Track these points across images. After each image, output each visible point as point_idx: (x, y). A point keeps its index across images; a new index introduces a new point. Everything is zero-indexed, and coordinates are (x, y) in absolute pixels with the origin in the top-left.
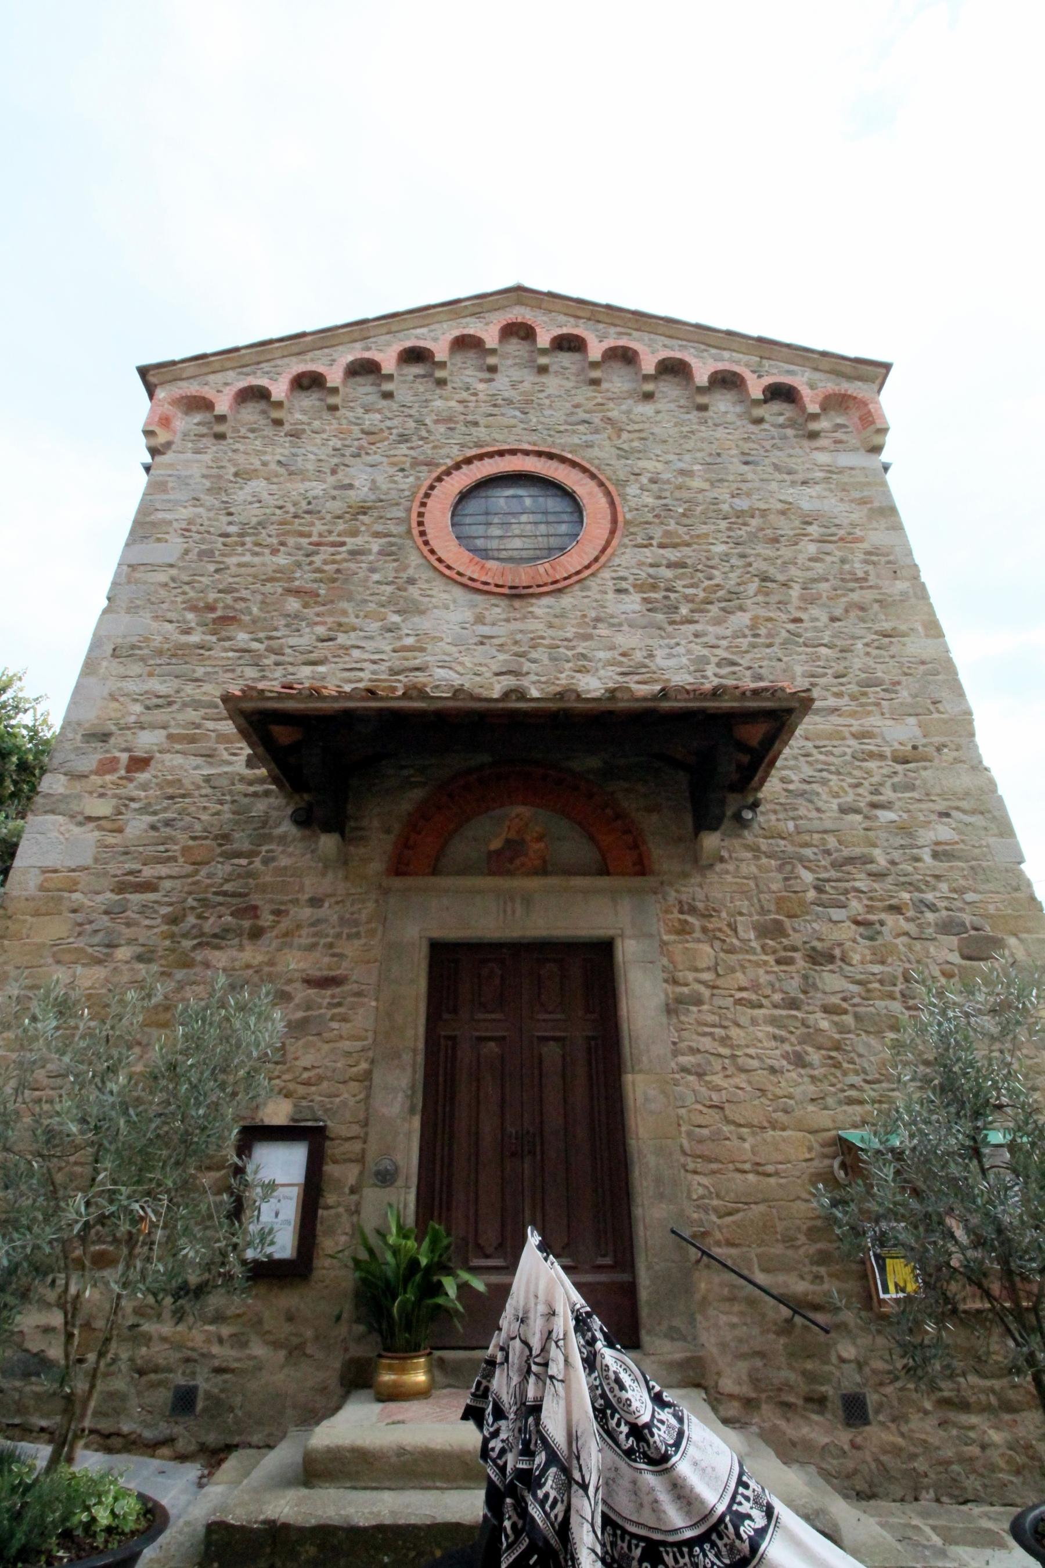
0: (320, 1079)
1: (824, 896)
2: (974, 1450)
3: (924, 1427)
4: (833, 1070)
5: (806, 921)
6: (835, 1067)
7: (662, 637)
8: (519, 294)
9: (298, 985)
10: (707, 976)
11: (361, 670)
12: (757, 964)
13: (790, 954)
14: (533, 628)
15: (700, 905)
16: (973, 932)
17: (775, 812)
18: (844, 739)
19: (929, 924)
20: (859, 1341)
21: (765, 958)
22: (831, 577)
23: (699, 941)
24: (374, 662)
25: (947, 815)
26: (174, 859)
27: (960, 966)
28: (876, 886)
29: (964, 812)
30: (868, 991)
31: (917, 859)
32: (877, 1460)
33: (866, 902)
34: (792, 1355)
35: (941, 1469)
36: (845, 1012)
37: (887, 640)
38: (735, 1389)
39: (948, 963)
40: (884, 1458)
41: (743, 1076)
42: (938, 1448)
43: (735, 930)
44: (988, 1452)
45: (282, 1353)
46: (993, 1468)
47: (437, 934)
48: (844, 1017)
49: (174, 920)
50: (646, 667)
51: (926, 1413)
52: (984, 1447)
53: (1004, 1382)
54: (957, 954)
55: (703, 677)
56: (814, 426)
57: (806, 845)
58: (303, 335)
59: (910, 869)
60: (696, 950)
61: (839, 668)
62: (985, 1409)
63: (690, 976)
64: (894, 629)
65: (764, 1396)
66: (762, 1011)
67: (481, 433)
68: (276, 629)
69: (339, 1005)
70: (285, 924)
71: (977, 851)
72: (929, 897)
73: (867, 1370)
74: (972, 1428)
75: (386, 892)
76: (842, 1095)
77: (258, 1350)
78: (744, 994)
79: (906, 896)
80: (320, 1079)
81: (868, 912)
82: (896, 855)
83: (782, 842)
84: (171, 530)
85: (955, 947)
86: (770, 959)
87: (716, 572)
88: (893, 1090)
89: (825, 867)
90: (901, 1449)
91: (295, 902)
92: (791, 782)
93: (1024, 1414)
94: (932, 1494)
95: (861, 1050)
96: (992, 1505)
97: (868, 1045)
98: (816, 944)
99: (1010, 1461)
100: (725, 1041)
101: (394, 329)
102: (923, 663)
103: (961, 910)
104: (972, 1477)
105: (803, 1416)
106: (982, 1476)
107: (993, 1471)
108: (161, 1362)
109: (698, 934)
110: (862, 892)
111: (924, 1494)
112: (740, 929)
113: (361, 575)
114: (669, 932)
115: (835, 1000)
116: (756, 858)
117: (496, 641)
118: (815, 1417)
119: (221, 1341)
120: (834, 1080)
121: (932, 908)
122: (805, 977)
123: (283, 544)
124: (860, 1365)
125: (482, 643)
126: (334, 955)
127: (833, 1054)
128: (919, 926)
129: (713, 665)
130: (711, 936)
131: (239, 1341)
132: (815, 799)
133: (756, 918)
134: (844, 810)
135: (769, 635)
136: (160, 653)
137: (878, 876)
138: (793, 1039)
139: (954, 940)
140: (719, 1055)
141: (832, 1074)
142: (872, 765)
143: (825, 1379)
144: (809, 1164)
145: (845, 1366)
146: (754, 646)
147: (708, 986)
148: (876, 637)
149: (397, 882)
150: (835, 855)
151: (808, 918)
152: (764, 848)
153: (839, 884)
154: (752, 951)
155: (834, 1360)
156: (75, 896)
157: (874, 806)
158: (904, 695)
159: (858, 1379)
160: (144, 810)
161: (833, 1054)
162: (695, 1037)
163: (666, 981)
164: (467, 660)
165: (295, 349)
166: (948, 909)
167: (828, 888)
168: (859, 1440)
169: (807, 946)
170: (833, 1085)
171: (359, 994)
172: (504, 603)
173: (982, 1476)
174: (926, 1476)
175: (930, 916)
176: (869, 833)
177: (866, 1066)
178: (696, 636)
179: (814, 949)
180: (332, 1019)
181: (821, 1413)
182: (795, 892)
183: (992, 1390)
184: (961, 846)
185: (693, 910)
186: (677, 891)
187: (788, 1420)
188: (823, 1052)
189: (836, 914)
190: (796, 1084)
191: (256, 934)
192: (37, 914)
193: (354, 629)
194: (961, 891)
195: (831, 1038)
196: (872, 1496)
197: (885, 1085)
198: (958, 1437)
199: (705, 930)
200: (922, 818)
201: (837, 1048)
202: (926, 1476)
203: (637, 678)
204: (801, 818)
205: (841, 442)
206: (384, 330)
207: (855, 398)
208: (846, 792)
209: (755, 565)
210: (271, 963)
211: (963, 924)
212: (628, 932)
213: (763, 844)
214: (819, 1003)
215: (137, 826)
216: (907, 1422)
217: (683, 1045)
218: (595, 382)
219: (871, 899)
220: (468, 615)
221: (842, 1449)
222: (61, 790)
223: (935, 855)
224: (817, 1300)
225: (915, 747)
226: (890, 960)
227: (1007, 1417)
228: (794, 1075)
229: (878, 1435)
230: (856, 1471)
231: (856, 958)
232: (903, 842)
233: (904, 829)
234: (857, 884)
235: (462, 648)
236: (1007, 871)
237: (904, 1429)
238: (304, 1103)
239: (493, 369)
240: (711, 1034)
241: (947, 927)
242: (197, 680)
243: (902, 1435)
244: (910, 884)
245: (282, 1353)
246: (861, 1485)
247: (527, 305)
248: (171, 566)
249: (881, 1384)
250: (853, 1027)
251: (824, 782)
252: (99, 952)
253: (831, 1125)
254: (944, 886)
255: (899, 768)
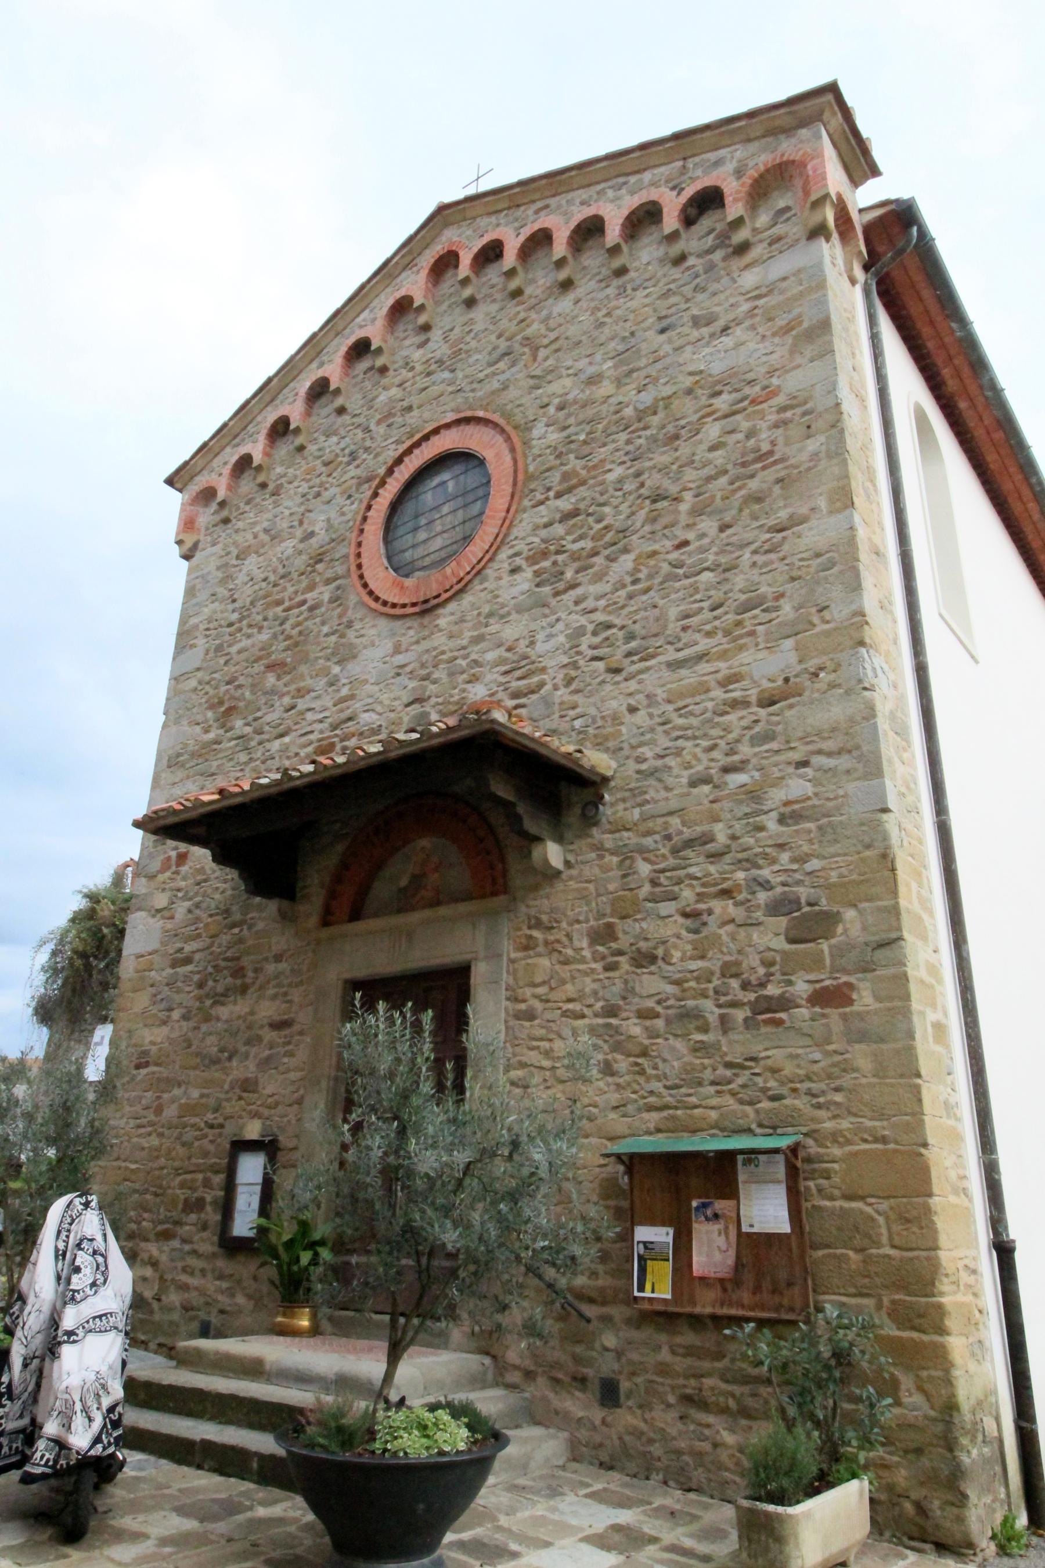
0: (277, 1104)
1: (658, 889)
2: (706, 1446)
3: (666, 1419)
4: (637, 1077)
5: (636, 920)
6: (639, 1073)
7: (546, 616)
8: (444, 215)
9: (267, 1029)
10: (541, 990)
11: (312, 732)
12: (586, 974)
13: (616, 959)
14: (962, 1255)
15: (544, 918)
16: (806, 909)
17: (624, 800)
18: (708, 690)
19: (759, 906)
20: (621, 1334)
21: (594, 966)
22: (729, 467)
23: (540, 955)
24: (321, 721)
25: (805, 764)
26: (199, 936)
27: (784, 953)
28: (712, 869)
29: (830, 754)
30: (684, 991)
31: (761, 828)
32: (620, 1438)
33: (699, 890)
34: (564, 1338)
35: (673, 1457)
36: (657, 1016)
37: (780, 535)
38: (517, 1361)
39: (770, 949)
40: (627, 1438)
41: (560, 1087)
42: (674, 1438)
43: (571, 939)
44: (719, 1450)
45: (252, 1302)
46: (721, 1467)
47: (347, 976)
48: (656, 1021)
49: (201, 985)
50: (527, 658)
51: (669, 1406)
52: (715, 1445)
53: (747, 1389)
54: (782, 937)
55: (578, 653)
56: (742, 235)
57: (649, 833)
58: (270, 380)
59: (752, 841)
60: (535, 965)
61: (717, 595)
62: (724, 1411)
63: (528, 992)
64: (791, 517)
65: (540, 1370)
66: (586, 1021)
67: (413, 418)
68: (259, 710)
69: (289, 1043)
70: (262, 979)
71: (831, 804)
72: (766, 873)
73: (624, 1360)
74: (708, 1426)
75: (318, 942)
76: (641, 1102)
77: (240, 1299)
78: (570, 1006)
79: (741, 875)
80: (277, 1104)
81: (697, 902)
82: (738, 826)
83: (625, 834)
84: (198, 634)
85: (783, 930)
86: (598, 966)
87: (607, 510)
88: (690, 1095)
89: (663, 856)
90: (642, 1433)
91: (266, 959)
92: (645, 760)
93: (759, 1422)
94: (661, 1476)
95: (667, 1055)
96: (712, 1497)
97: (673, 1049)
98: (643, 945)
99: (738, 1464)
100: (547, 1054)
101: (340, 328)
102: (818, 555)
103: (799, 883)
104: (700, 1470)
105: (569, 1392)
106: (709, 1471)
107: (719, 1469)
108: (195, 1304)
109: (541, 949)
110: (697, 878)
111: (654, 1476)
112: (575, 937)
113: (316, 630)
114: (517, 949)
115: (650, 1003)
116: (601, 857)
117: (408, 669)
118: (578, 1394)
119: (222, 1293)
120: (637, 1087)
121: (766, 886)
122: (626, 982)
123: (265, 619)
124: (619, 1354)
125: (398, 674)
126: (287, 1002)
127: (640, 1060)
128: (748, 910)
129: (588, 636)
130: (551, 948)
131: (231, 1293)
132: (665, 776)
133: (592, 923)
134: (693, 784)
135: (650, 577)
136: (193, 755)
137: (714, 857)
138: (606, 1047)
139: (783, 922)
140: (541, 1068)
141: (636, 1081)
142: (732, 718)
143: (589, 1363)
144: (603, 1169)
145: (607, 1354)
146: (630, 597)
147: (542, 1001)
148: (768, 536)
149: (325, 933)
150: (676, 839)
151: (638, 917)
152: (608, 845)
153: (674, 873)
154: (583, 960)
155: (597, 1345)
156: (153, 973)
157: (726, 770)
158: (787, 609)
159: (616, 1367)
160: (186, 898)
161: (640, 1060)
162: (525, 1051)
163: (508, 999)
164: (385, 697)
165: (268, 398)
166: (784, 884)
167: (662, 880)
168: (609, 1419)
169: (634, 948)
170: (635, 1092)
171: (301, 1033)
172: (414, 623)
173: (709, 1471)
174: (659, 1459)
175: (762, 897)
176: (714, 805)
177: (667, 1071)
178: (576, 603)
179: (639, 950)
180: (285, 1055)
181: (583, 1390)
182: (631, 890)
183: (733, 1396)
184: (815, 802)
185: (538, 924)
186: (528, 906)
187: (556, 1393)
188: (631, 1059)
189: (667, 908)
190: (599, 1092)
191: (244, 990)
192: (135, 991)
193: (309, 692)
194: (802, 860)
195: (641, 1044)
196: (611, 1468)
197: (683, 1090)
198: (694, 1432)
199: (546, 943)
200: (778, 775)
201: (644, 1053)
202: (659, 1459)
203: (518, 673)
204: (648, 802)
205: (779, 239)
206: (333, 333)
207: (793, 162)
208: (699, 760)
209: (648, 483)
210: (252, 1013)
211: (797, 901)
212: (482, 954)
213: (609, 840)
214: (634, 1008)
215: (181, 909)
216: (651, 1410)
217: (514, 1061)
218: (517, 293)
219: (704, 885)
220: (388, 645)
221: (593, 1424)
222: (144, 891)
223: (782, 820)
224: (594, 1294)
225: (787, 680)
226: (710, 954)
227: (744, 1422)
228: (601, 1084)
229: (626, 1418)
230: (601, 1445)
231: (677, 955)
232: (748, 810)
233: (753, 794)
234: (692, 870)
235: (382, 686)
236: (862, 824)
237: (647, 1416)
238: (268, 1123)
239: (426, 328)
240: (538, 1048)
241: (775, 908)
242: (213, 774)
243: (645, 1421)
244: (747, 860)
245: (252, 1302)
246: (604, 1457)
247: (452, 224)
248: (198, 669)
249: (634, 1374)
250: (662, 1031)
251: (679, 752)
252: (163, 1015)
253: (627, 1132)
254: (785, 857)
255: (762, 712)
